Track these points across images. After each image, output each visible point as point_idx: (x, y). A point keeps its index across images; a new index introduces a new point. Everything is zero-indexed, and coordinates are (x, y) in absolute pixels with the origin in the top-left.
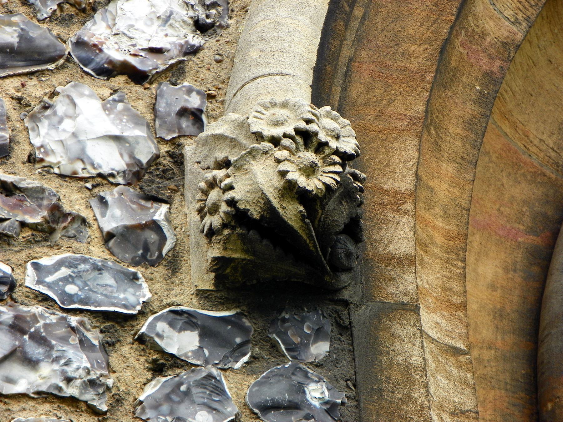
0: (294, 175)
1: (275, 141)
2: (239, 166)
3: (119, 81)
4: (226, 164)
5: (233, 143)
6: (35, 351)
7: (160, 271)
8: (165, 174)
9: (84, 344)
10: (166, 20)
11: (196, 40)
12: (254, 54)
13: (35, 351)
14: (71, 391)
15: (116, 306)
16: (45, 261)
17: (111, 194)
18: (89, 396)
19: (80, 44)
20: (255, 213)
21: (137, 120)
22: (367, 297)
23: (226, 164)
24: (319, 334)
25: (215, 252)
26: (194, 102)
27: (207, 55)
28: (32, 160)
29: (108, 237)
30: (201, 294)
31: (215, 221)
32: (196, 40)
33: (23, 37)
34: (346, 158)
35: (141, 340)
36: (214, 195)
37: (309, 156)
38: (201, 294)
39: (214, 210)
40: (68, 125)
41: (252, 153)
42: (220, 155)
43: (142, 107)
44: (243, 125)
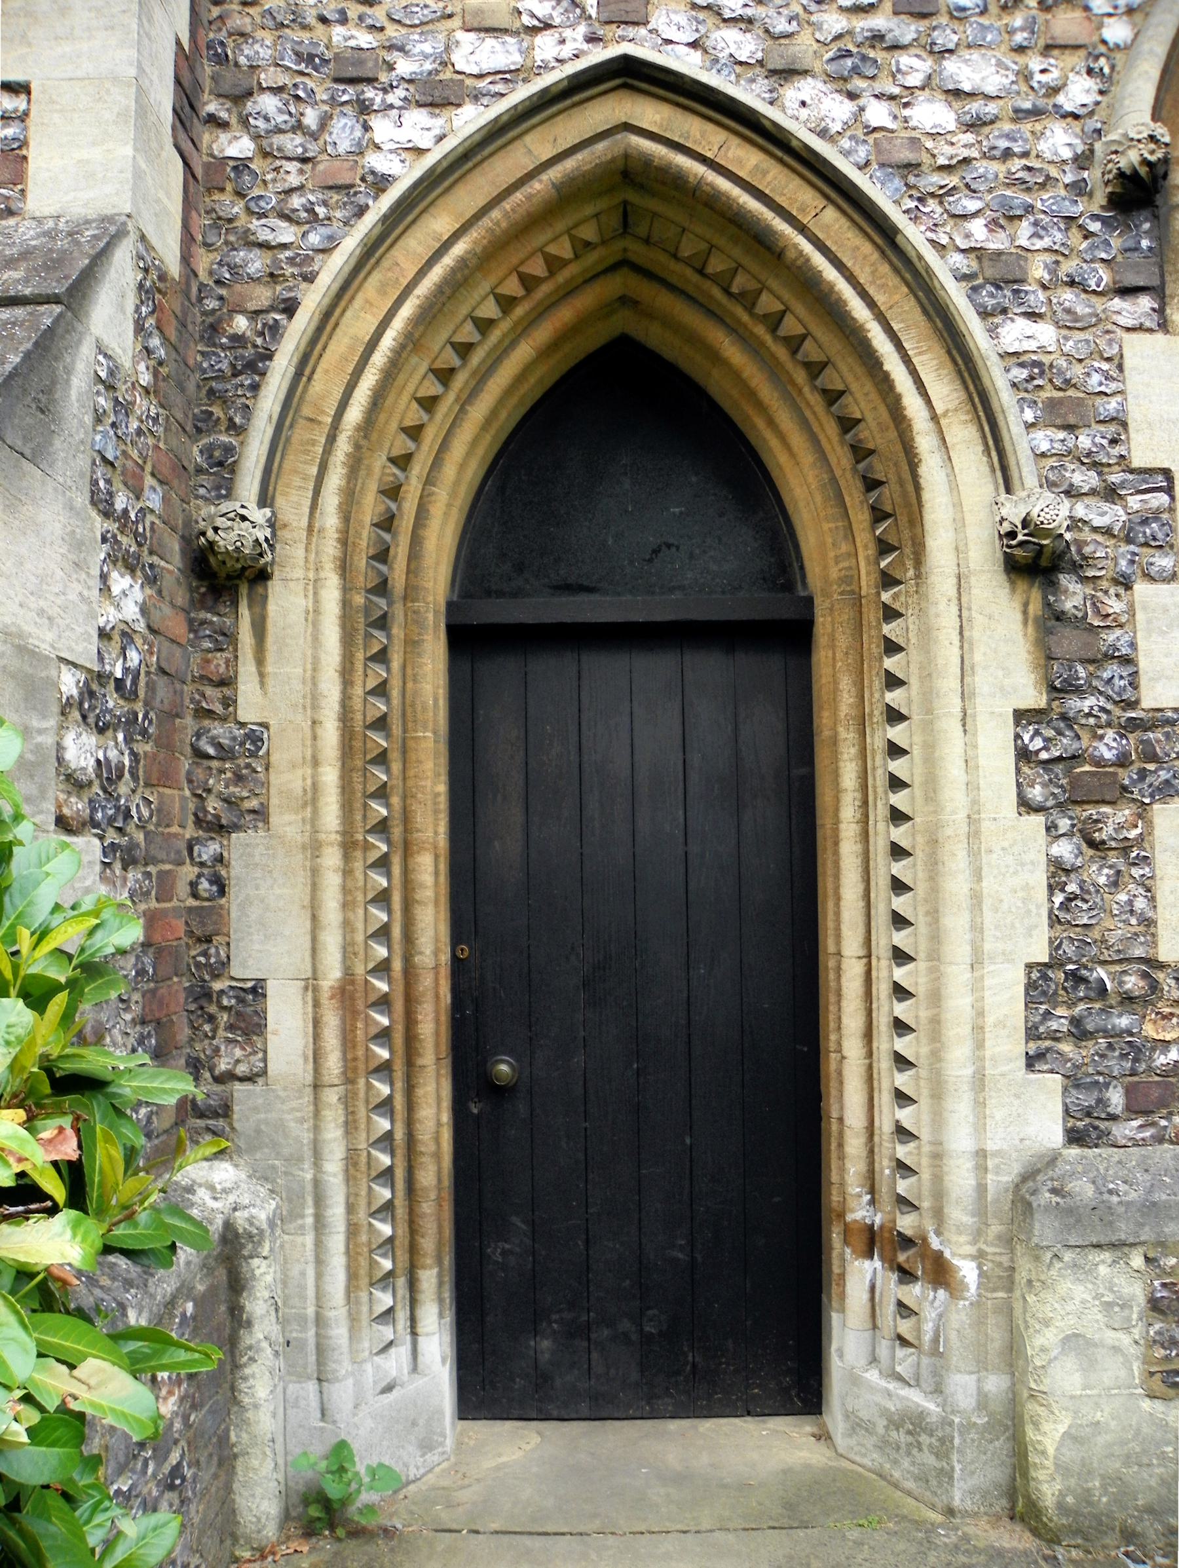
0: (1147, 155)
1: (1139, 141)
2: (1123, 153)
3: (1069, 120)
4: (1116, 152)
5: (1119, 143)
6: (1042, 233)
7: (1085, 198)
8: (1087, 158)
9: (1059, 229)
10: (1088, 91)
11: (1099, 98)
12: (1127, 102)
13: (1042, 233)
14: (1056, 247)
15: (417, 204)
16: (1045, 197)
17: (1067, 168)
18: (1062, 249)
19: (1055, 106)
20: (1128, 172)
21: (1076, 136)
22: (1166, 203)
23: (1116, 152)
24: (1146, 220)
25: (1109, 189)
26: (1099, 125)
27: (1103, 105)
28: (1038, 156)
29: (1066, 186)
30: (1102, 207)
31: (1111, 176)
32: (1099, 98)
33: (1034, 105)
34: (1167, 145)
35: (1080, 226)
36: (1110, 166)
37: (1152, 146)
38: (1102, 207)
39: (1110, 172)
40: (1051, 141)
41: (1129, 147)
42: (1113, 148)
43: (1078, 130)
44: (1125, 135)
